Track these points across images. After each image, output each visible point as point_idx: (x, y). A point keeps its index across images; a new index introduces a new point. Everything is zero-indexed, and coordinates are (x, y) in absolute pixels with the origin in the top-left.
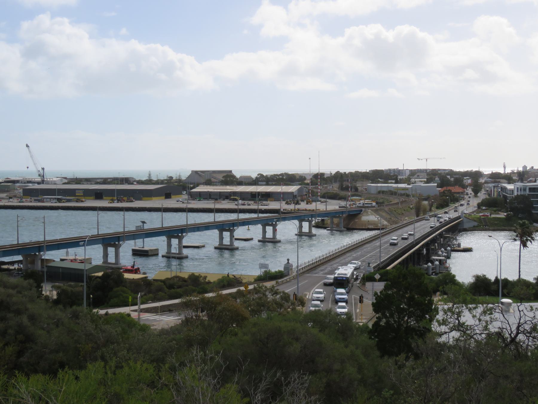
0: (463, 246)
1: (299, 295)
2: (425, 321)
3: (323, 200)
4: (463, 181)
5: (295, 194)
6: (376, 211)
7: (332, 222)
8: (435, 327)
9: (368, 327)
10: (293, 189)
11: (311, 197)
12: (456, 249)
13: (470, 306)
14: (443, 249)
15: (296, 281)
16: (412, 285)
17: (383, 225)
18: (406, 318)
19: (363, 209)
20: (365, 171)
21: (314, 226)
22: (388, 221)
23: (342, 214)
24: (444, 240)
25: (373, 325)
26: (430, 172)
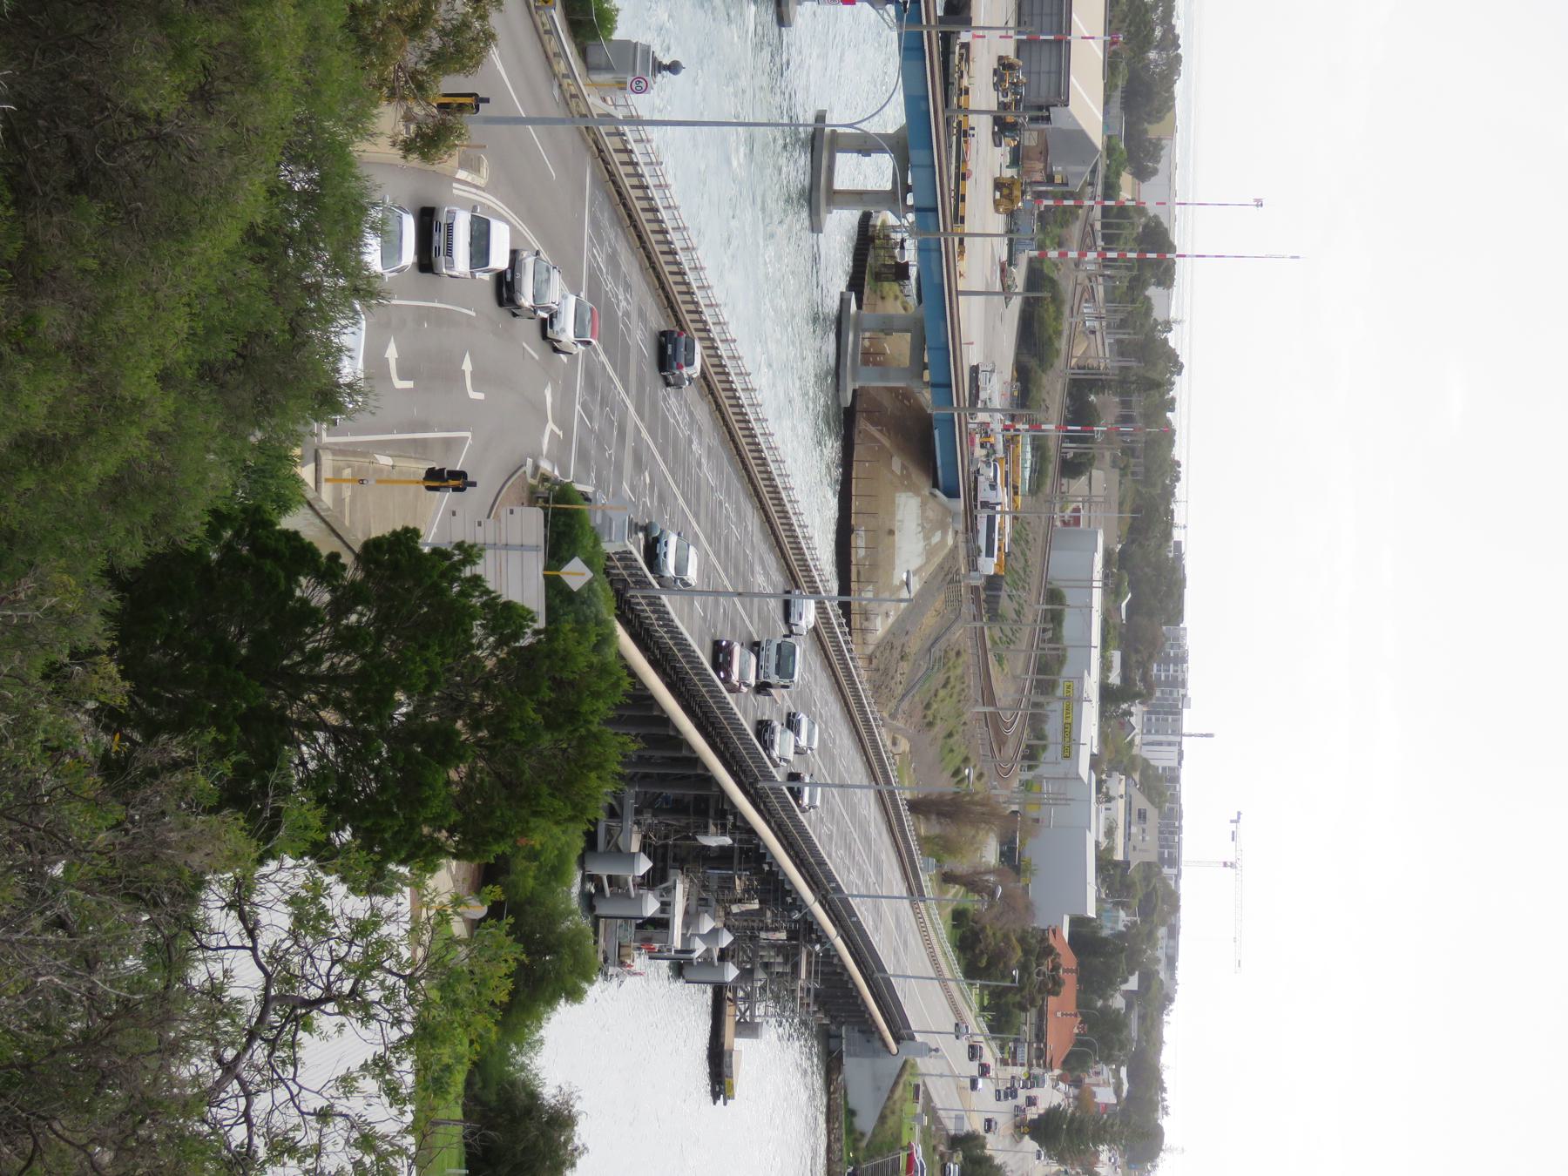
0: (742, 1050)
1: (472, 126)
2: (315, 818)
3: (1019, 275)
4: (1108, 1060)
5: (1054, 112)
6: (945, 576)
7: (888, 327)
8: (285, 875)
9: (284, 507)
10: (1087, 104)
11: (1038, 206)
12: (729, 1010)
13: (407, 1065)
14: (726, 939)
15: (554, 111)
16: (523, 752)
17: (866, 615)
18: (331, 717)
19: (960, 504)
20: (1179, 518)
21: (865, 220)
22: (887, 644)
23: (934, 385)
24: (778, 948)
25: (293, 537)
26: (1164, 881)
